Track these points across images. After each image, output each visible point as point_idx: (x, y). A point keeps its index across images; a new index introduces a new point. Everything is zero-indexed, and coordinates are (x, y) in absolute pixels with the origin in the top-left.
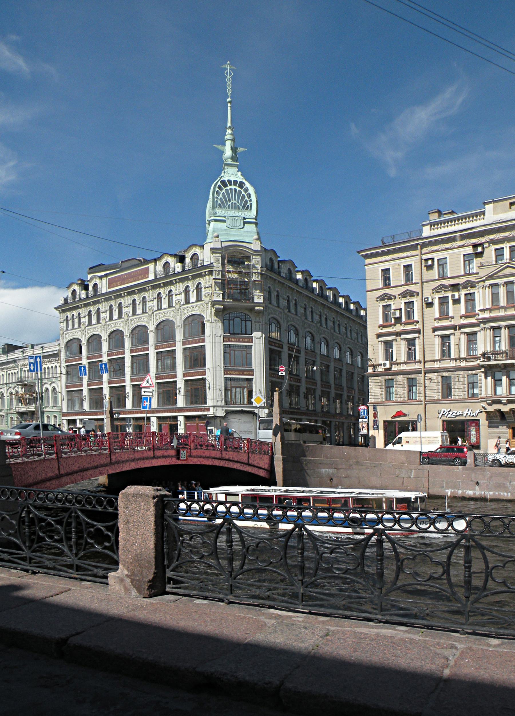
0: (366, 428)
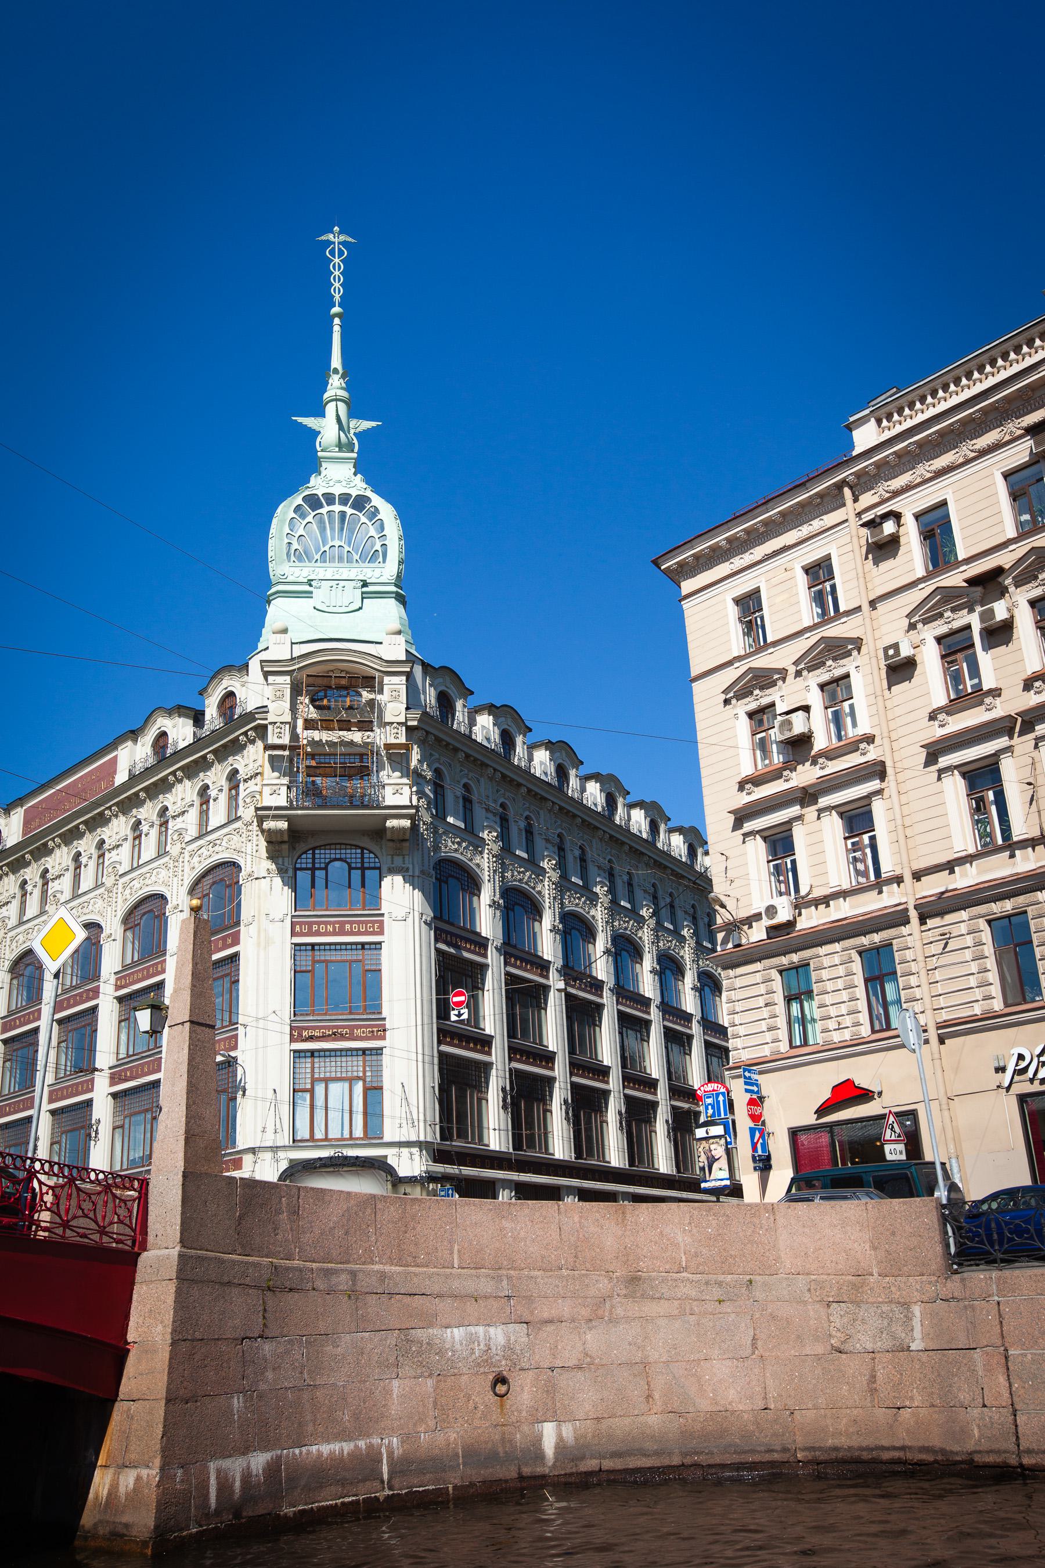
0: (723, 1163)
